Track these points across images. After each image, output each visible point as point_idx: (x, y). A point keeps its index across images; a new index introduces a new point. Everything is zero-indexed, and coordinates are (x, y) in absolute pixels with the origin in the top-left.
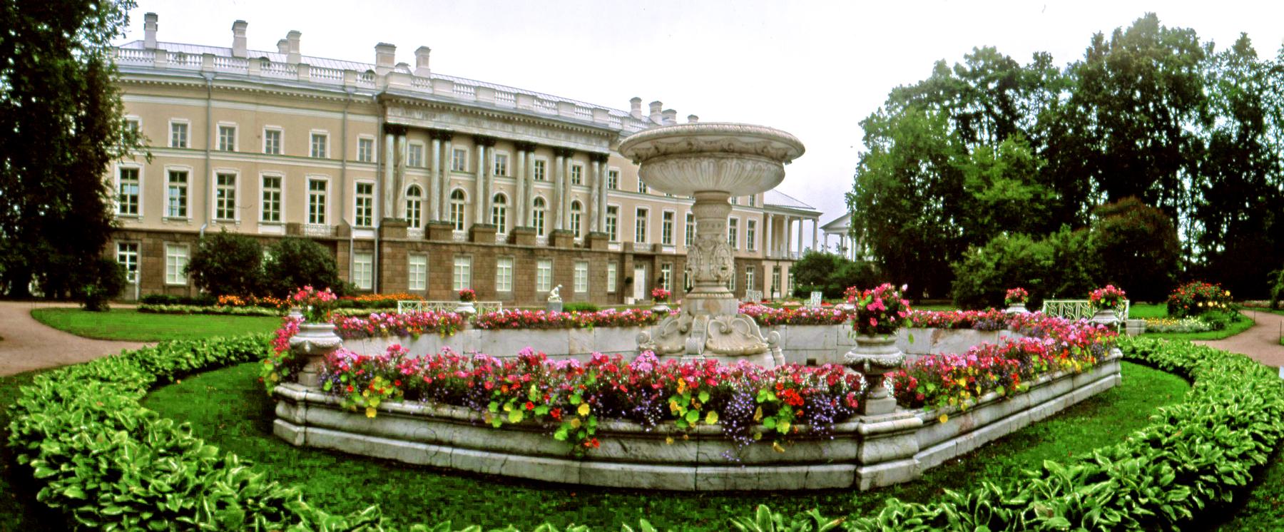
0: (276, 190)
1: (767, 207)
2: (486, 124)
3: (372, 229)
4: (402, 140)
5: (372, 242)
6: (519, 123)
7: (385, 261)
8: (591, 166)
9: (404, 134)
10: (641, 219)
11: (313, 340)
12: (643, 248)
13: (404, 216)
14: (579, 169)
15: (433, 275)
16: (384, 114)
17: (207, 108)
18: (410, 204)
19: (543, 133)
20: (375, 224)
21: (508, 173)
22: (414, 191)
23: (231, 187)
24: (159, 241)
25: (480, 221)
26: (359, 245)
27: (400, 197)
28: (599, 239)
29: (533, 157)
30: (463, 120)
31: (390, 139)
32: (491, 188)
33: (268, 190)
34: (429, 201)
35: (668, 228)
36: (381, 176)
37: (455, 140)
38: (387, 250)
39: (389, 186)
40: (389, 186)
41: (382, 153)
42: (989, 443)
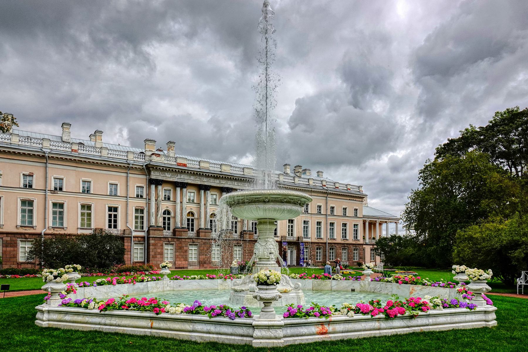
0: (115, 213)
1: (364, 217)
2: (205, 179)
3: (144, 231)
4: (160, 187)
5: (143, 238)
7: (151, 247)
8: (149, 187)
9: (161, 185)
10: (291, 224)
11: (52, 286)
12: (290, 239)
13: (161, 224)
15: (177, 254)
16: (149, 174)
18: (164, 219)
20: (146, 229)
21: (172, 199)
22: (167, 212)
23: (115, 213)
24: (14, 239)
25: (203, 226)
26: (137, 239)
27: (159, 216)
30: (192, 178)
32: (208, 211)
34: (175, 217)
35: (306, 229)
36: (149, 205)
37: (188, 187)
38: (152, 242)
39: (153, 210)
40: (153, 210)
41: (149, 194)
42: (78, 331)
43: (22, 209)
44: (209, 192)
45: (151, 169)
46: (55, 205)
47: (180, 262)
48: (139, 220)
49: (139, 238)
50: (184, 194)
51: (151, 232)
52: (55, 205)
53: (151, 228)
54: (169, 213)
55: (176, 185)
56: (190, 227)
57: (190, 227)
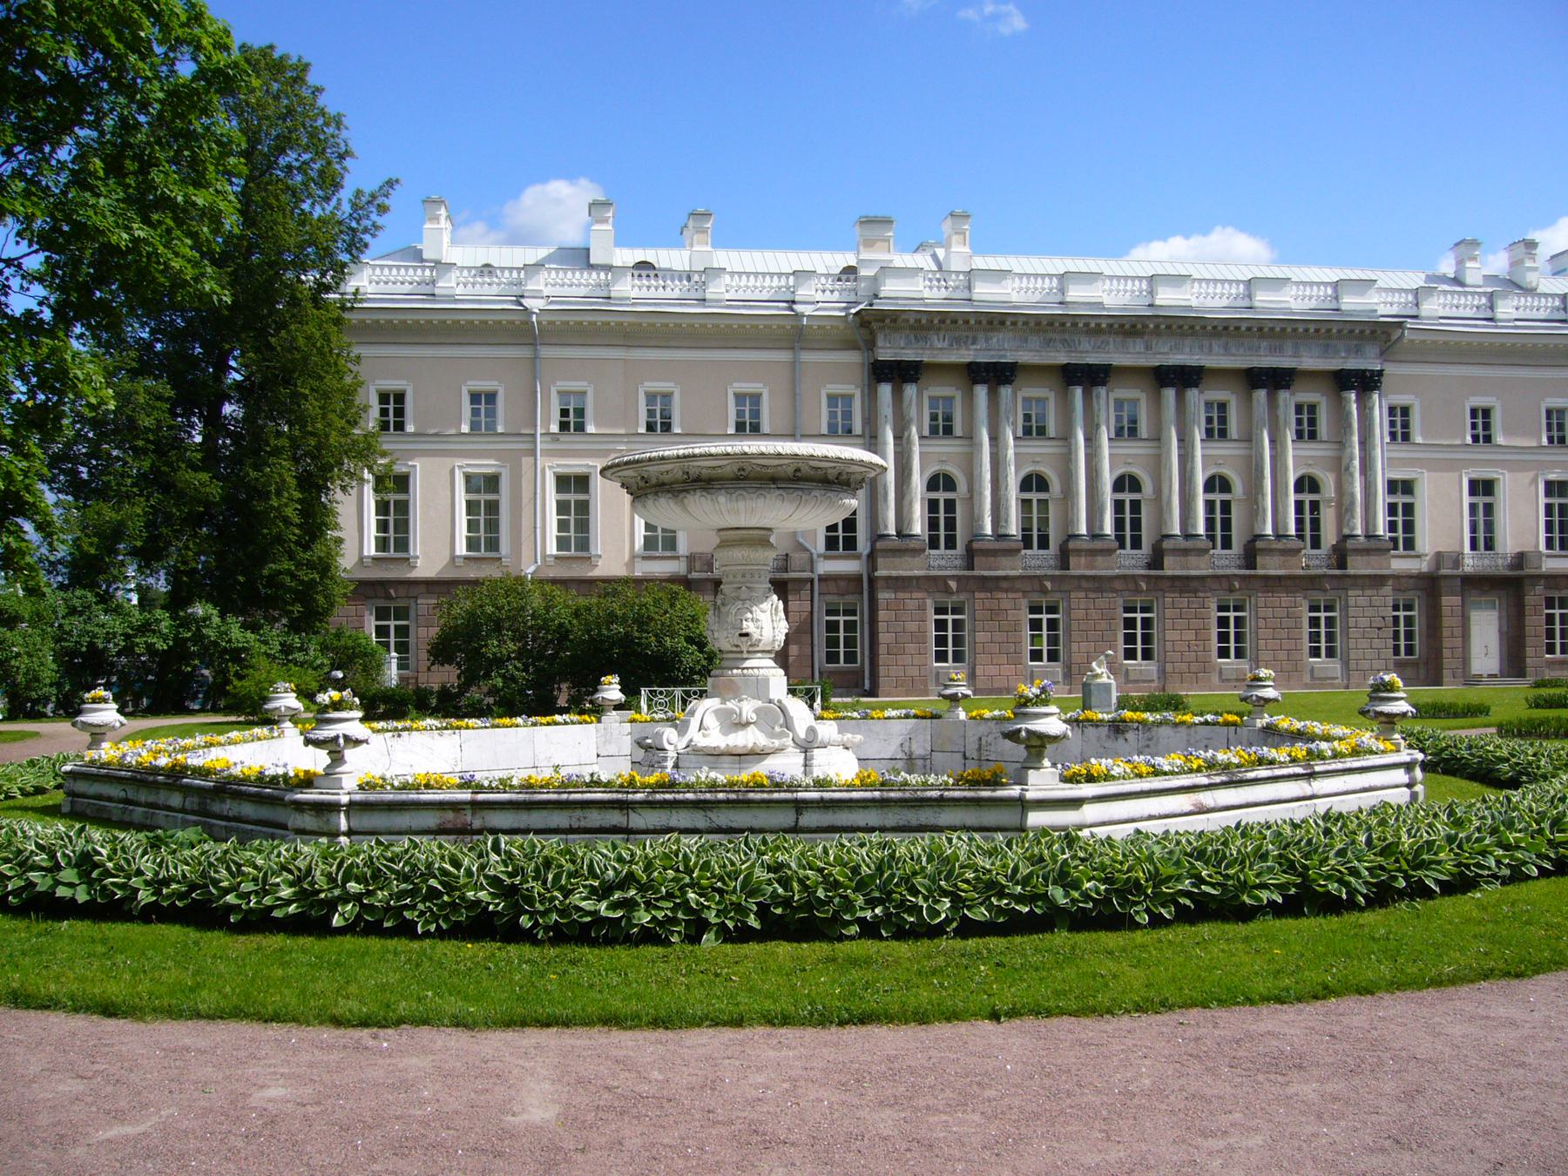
5: (855, 579)
6: (1157, 332)
7: (882, 615)
8: (1157, 402)
9: (915, 380)
10: (1481, 500)
12: (1471, 563)
13: (918, 527)
14: (1312, 408)
16: (871, 345)
17: (794, 364)
19: (1217, 345)
21: (958, 430)
26: (832, 587)
28: (1367, 552)
29: (1196, 398)
30: (1035, 342)
31: (885, 390)
33: (1120, 496)
38: (883, 596)
43: (558, 502)
44: (1102, 391)
45: (874, 325)
46: (563, 482)
47: (993, 670)
48: (572, 518)
49: (842, 584)
50: (1003, 408)
51: (880, 561)
52: (1392, 486)
53: (879, 545)
54: (950, 484)
55: (977, 373)
56: (1218, 533)
57: (1218, 533)
